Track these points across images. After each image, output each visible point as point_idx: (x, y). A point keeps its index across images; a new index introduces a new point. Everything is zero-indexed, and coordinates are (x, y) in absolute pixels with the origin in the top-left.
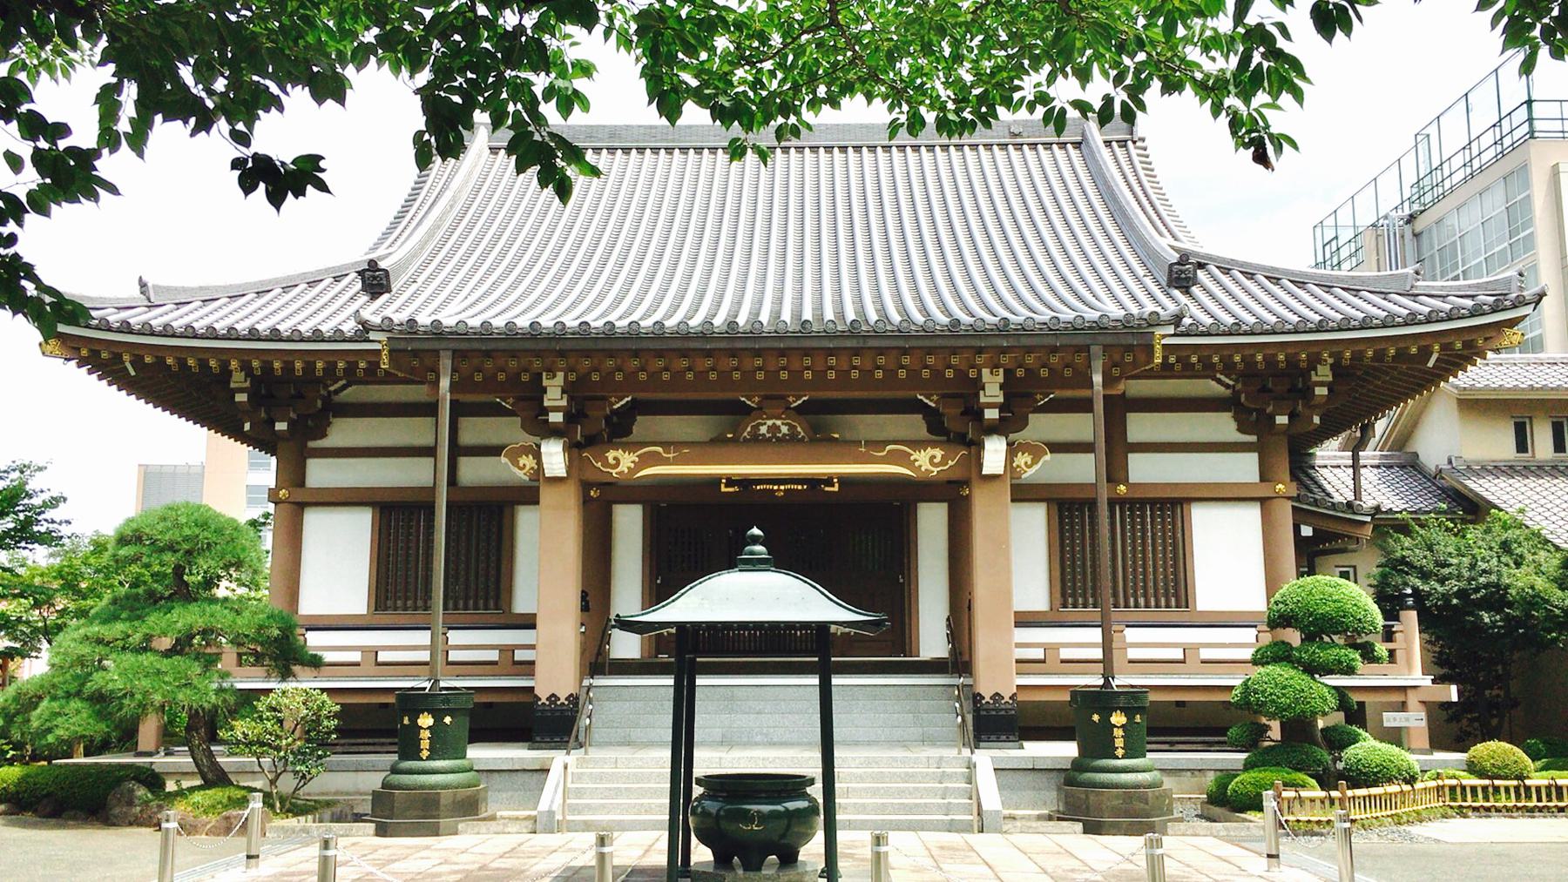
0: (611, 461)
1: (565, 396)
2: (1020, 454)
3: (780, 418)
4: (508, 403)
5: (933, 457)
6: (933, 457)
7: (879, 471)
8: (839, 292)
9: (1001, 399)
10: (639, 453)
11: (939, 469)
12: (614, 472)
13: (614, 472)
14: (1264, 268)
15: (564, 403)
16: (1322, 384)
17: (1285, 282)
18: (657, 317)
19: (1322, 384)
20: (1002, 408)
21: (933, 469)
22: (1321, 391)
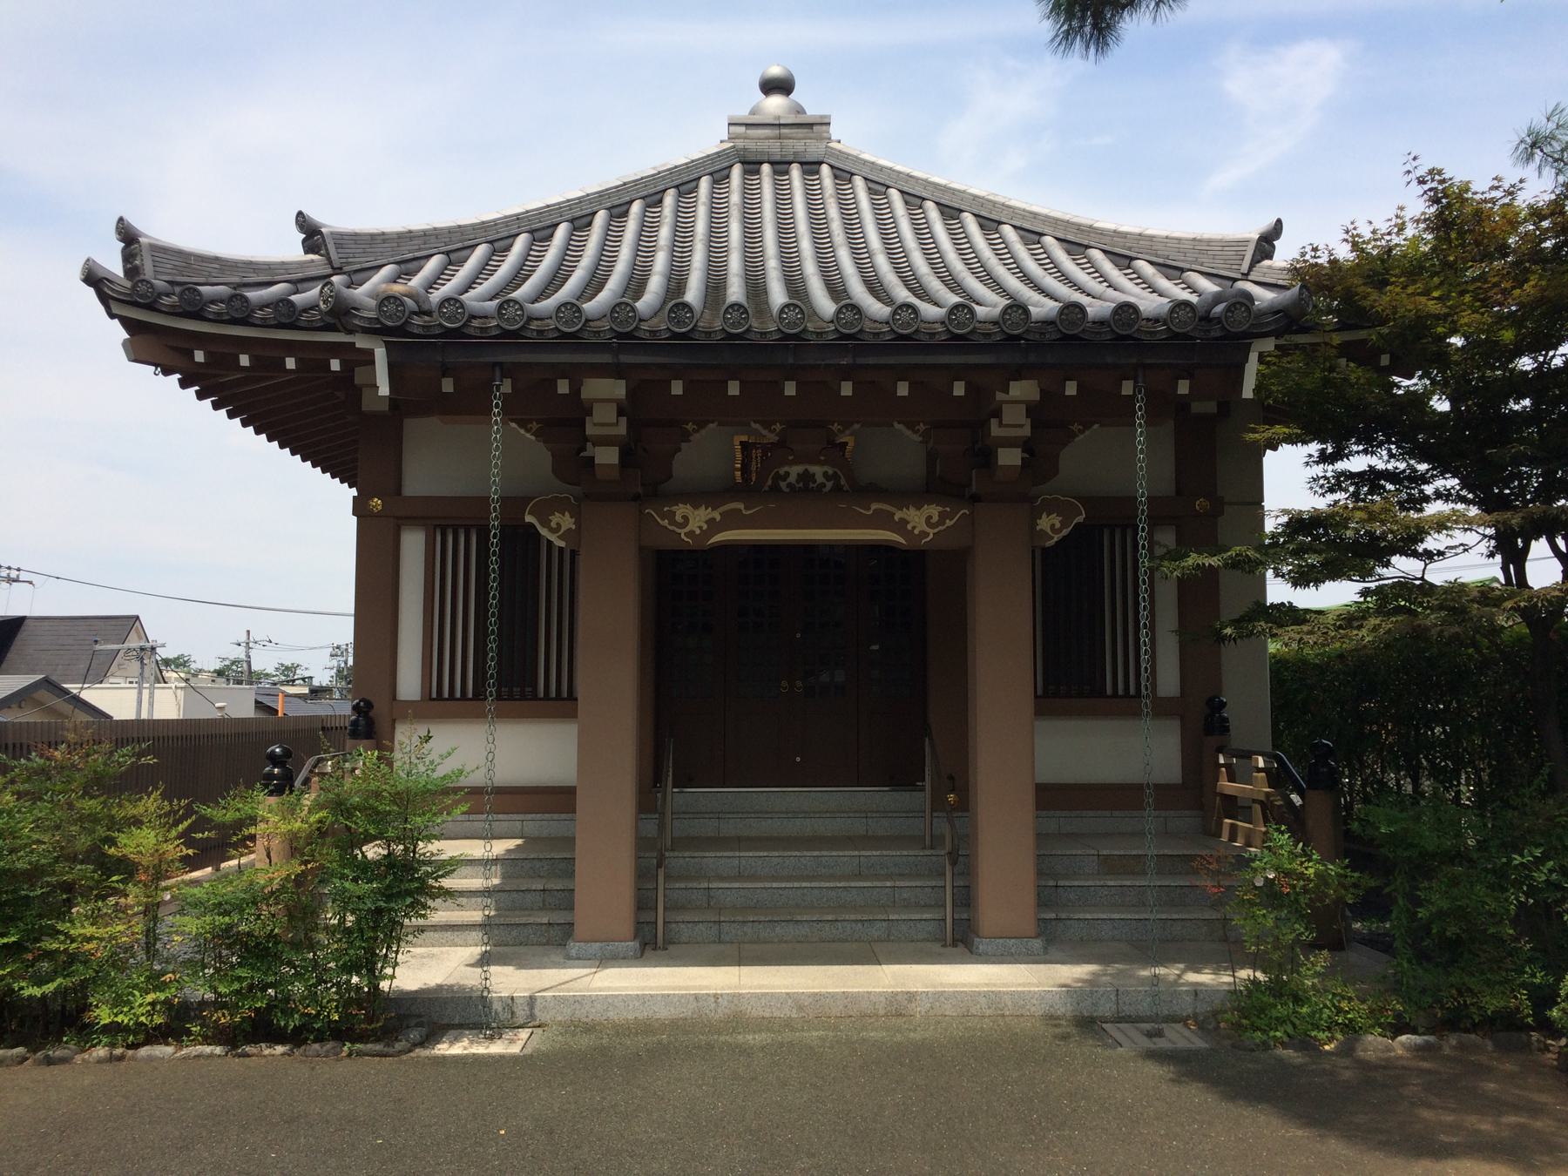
0: (678, 518)
1: (624, 420)
2: (1044, 516)
3: (820, 463)
4: (528, 431)
5: (930, 517)
6: (930, 517)
7: (817, 537)
8: (751, 234)
9: (1026, 431)
10: (722, 509)
11: (936, 530)
12: (682, 532)
13: (682, 532)
14: (1056, 222)
15: (622, 429)
16: (1009, 443)
17: (1096, 255)
18: (447, 289)
19: (1009, 443)
20: (1027, 446)
21: (928, 530)
22: (1010, 458)
